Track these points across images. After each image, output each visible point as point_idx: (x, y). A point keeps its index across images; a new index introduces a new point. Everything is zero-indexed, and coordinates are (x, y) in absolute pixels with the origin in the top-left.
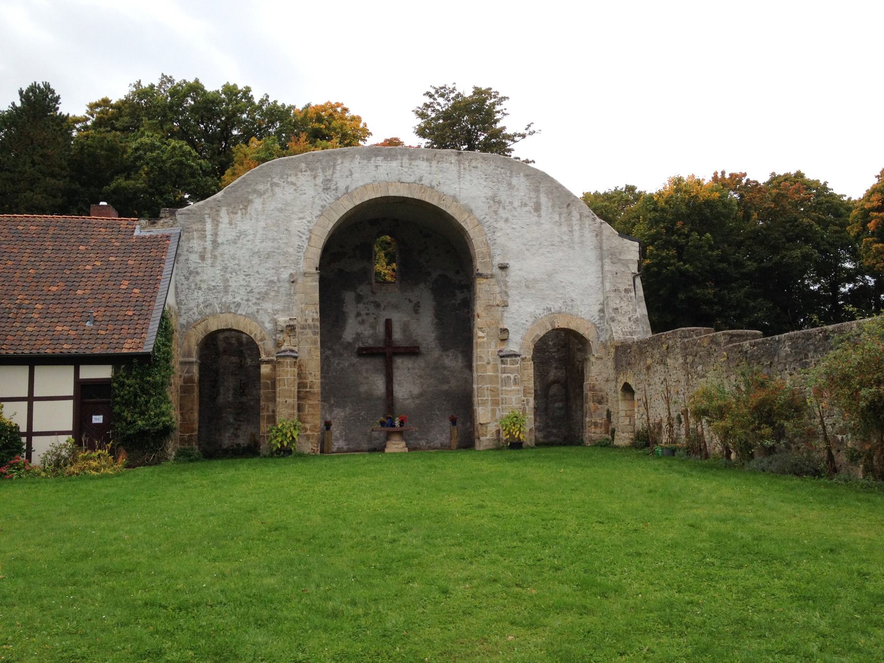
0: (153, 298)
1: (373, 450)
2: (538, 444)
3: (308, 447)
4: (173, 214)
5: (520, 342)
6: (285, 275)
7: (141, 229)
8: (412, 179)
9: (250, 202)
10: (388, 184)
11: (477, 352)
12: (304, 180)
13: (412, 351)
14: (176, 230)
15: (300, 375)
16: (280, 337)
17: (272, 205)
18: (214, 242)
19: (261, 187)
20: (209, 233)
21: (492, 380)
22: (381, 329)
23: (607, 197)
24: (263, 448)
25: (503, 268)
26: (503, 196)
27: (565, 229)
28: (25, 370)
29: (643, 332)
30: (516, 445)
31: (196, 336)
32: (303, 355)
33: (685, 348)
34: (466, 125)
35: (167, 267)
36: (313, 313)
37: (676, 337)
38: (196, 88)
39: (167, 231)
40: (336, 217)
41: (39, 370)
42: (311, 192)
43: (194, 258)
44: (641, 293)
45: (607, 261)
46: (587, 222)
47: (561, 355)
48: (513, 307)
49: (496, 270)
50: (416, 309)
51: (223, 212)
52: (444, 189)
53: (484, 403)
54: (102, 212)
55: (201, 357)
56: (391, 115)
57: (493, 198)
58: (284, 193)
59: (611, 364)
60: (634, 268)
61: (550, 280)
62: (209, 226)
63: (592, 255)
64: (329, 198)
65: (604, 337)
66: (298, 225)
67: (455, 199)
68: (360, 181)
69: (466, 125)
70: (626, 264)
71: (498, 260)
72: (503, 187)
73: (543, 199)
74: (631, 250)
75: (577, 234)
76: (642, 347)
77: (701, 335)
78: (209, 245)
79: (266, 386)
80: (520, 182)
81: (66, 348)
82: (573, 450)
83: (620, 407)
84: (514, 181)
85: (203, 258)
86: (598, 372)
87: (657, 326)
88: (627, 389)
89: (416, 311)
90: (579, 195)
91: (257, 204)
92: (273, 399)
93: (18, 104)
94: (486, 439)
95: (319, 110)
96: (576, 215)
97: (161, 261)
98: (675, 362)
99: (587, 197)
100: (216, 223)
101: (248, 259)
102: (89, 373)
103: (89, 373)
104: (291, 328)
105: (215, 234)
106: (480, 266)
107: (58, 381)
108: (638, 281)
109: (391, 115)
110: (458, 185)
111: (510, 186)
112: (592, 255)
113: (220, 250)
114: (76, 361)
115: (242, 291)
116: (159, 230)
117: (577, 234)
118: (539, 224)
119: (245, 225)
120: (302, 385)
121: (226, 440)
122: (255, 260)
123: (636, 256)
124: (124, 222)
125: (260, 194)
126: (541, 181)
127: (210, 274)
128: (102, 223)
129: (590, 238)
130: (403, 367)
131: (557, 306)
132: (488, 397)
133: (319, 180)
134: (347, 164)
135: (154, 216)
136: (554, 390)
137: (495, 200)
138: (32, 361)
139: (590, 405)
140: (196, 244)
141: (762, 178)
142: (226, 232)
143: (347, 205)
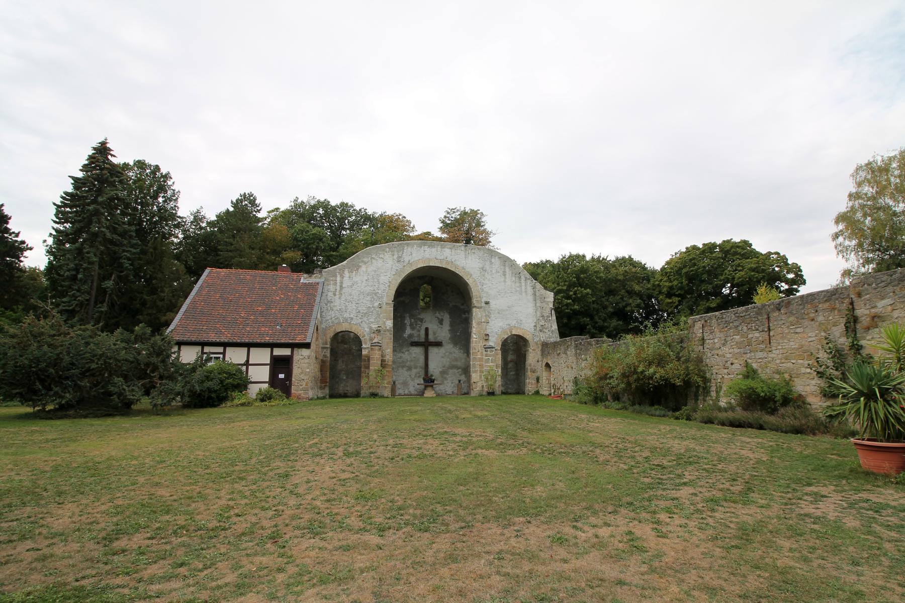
0: (311, 315)
1: (465, 394)
2: (503, 393)
3: (387, 392)
4: (321, 272)
5: (495, 341)
6: (376, 304)
7: (304, 279)
8: (442, 258)
9: (360, 267)
10: (430, 260)
11: (473, 345)
12: (387, 256)
13: (438, 344)
14: (323, 280)
15: (382, 356)
16: (373, 335)
17: (371, 269)
18: (341, 286)
19: (365, 260)
20: (338, 282)
21: (481, 360)
22: (423, 332)
23: (537, 266)
24: (362, 393)
25: (487, 303)
26: (487, 267)
27: (518, 284)
28: (246, 349)
29: (555, 337)
30: (491, 394)
31: (331, 334)
32: (384, 346)
33: (576, 346)
34: (465, 229)
35: (318, 299)
36: (390, 324)
37: (571, 340)
38: (325, 205)
39: (317, 280)
40: (403, 276)
41: (228, 349)
42: (391, 263)
43: (330, 294)
44: (554, 318)
45: (538, 301)
46: (529, 281)
47: (515, 348)
48: (491, 323)
49: (483, 305)
50: (441, 322)
51: (346, 272)
52: (458, 263)
53: (476, 372)
54: (284, 269)
55: (331, 345)
56: (426, 220)
57: (482, 268)
58: (377, 263)
59: (539, 353)
60: (551, 306)
61: (511, 310)
62: (338, 279)
63: (530, 298)
64: (400, 266)
65: (537, 339)
66: (384, 279)
67: (463, 268)
68: (419, 257)
69: (465, 229)
70: (547, 303)
71: (484, 300)
72: (488, 263)
73: (507, 269)
74: (550, 296)
75: (523, 287)
76: (555, 344)
77: (584, 339)
78: (338, 288)
79: (365, 360)
80: (496, 261)
81: (267, 339)
82: (520, 397)
83: (544, 375)
84: (493, 260)
85: (335, 295)
86: (533, 357)
87: (562, 335)
88: (548, 365)
89: (442, 324)
90: (521, 262)
91: (363, 268)
92: (368, 368)
93: (231, 209)
94: (476, 389)
95: (391, 218)
96: (523, 277)
97: (315, 296)
98: (571, 352)
99: (526, 266)
100: (342, 277)
101: (357, 297)
102: (278, 352)
103: (278, 352)
104: (379, 331)
105: (341, 283)
106: (474, 301)
107: (262, 356)
108: (553, 312)
109: (426, 220)
110: (461, 261)
111: (491, 263)
112: (531, 298)
113: (344, 290)
114: (272, 346)
115: (354, 312)
116: (313, 279)
117: (523, 287)
118: (505, 281)
119: (357, 278)
120: (383, 361)
121: (341, 389)
122: (361, 297)
123: (552, 300)
124: (295, 276)
125: (365, 263)
126: (505, 260)
127: (338, 303)
128: (284, 276)
129: (530, 291)
130: (433, 352)
131: (513, 323)
132: (478, 369)
133: (395, 257)
134: (409, 249)
135: (309, 272)
136: (510, 365)
137: (483, 269)
138: (249, 346)
139: (529, 373)
140: (332, 288)
141: (612, 258)
142: (347, 282)
143: (408, 270)
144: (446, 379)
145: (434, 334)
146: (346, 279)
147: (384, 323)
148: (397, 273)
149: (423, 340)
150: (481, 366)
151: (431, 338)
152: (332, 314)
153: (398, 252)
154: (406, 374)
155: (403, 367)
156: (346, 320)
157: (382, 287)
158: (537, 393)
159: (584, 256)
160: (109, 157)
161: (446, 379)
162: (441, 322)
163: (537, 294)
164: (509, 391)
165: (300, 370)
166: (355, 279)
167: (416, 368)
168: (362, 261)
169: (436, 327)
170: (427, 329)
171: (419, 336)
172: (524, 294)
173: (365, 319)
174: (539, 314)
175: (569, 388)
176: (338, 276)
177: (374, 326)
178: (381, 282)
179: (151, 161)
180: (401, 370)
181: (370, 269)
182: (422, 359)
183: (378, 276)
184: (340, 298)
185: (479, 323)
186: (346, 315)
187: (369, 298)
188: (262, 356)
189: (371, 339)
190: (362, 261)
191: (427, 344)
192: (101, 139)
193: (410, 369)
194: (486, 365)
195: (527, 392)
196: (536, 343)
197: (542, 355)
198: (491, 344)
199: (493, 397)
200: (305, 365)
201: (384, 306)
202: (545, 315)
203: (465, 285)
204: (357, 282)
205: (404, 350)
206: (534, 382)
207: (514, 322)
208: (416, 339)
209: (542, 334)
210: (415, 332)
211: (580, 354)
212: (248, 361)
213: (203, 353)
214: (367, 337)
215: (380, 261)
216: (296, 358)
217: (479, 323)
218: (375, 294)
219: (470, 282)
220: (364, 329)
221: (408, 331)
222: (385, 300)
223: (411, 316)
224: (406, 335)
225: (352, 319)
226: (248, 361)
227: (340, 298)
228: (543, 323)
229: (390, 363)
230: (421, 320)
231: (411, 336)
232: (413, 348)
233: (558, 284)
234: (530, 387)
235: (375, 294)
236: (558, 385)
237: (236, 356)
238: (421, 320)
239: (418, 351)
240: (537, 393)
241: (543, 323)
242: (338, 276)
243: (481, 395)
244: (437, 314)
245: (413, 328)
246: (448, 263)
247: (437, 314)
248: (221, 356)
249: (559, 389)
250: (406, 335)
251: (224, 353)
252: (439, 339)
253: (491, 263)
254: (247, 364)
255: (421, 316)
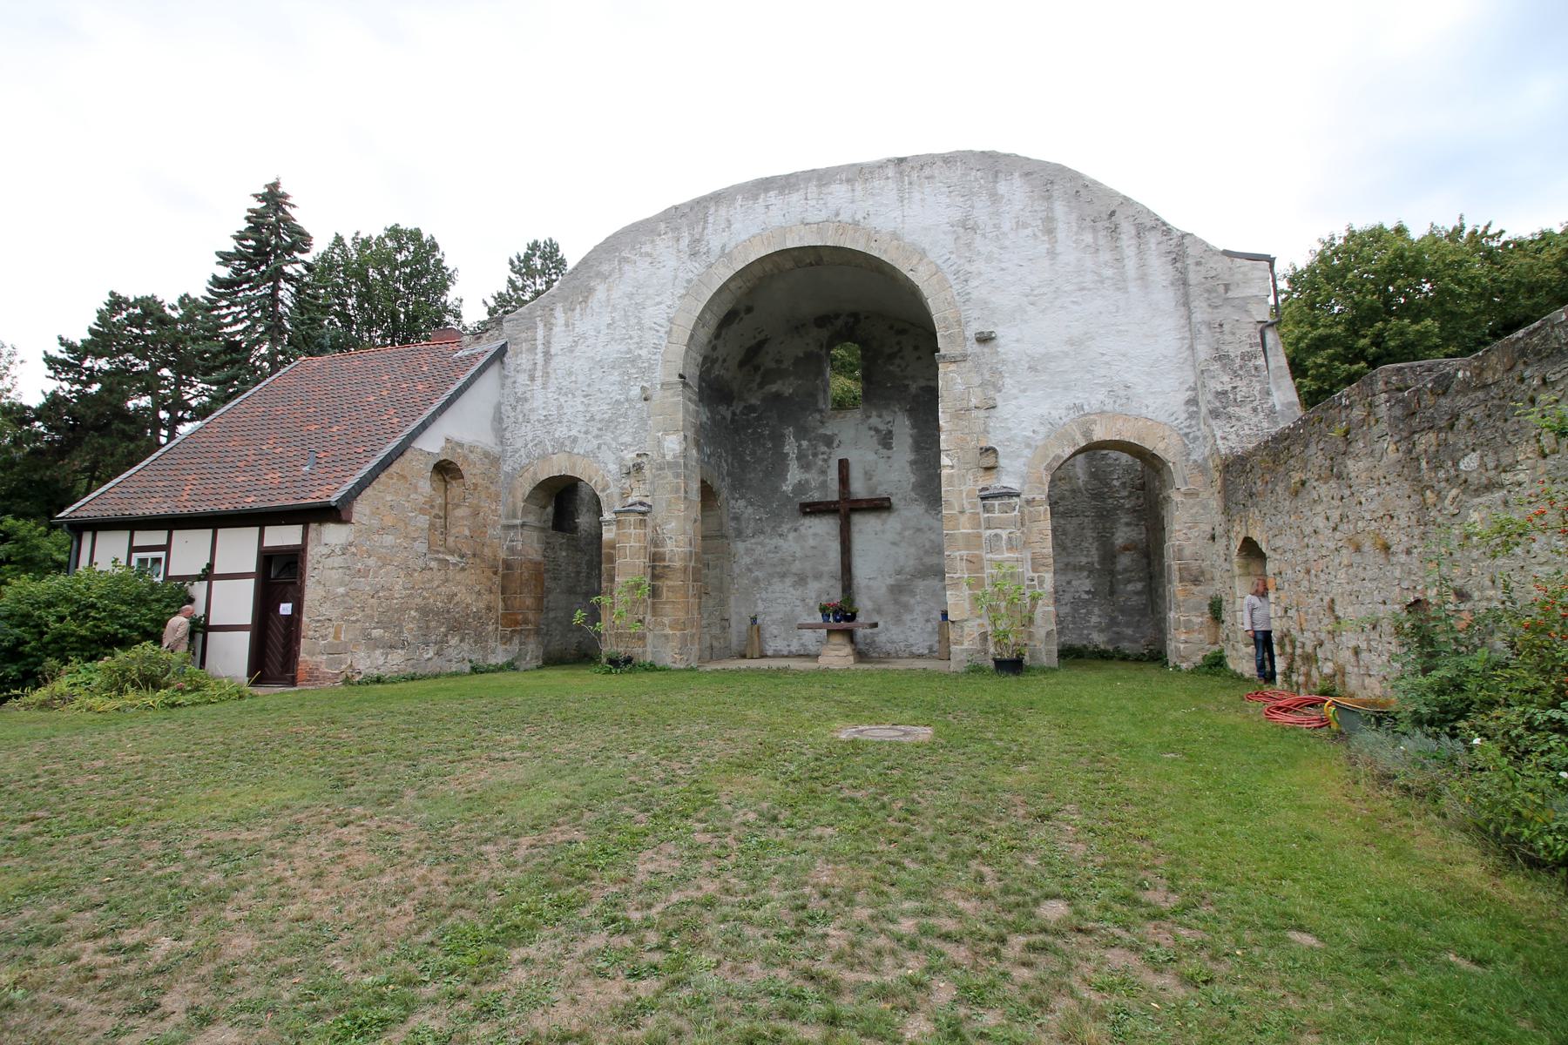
2: (1071, 655)
5: (1021, 472)
6: (635, 392)
8: (823, 216)
9: (591, 290)
10: (784, 231)
13: (880, 506)
16: (627, 483)
18: (547, 353)
20: (539, 342)
22: (834, 474)
25: (985, 339)
26: (981, 214)
27: (1105, 256)
30: (1012, 666)
31: (525, 486)
41: (176, 533)
43: (523, 378)
47: (1112, 499)
48: (1005, 409)
49: (973, 347)
50: (886, 440)
52: (876, 222)
59: (1215, 503)
62: (540, 333)
64: (697, 267)
66: (655, 314)
71: (971, 332)
73: (1060, 209)
75: (1131, 264)
78: (540, 358)
81: (251, 502)
84: (1002, 187)
85: (532, 379)
86: (1191, 524)
88: (1251, 549)
91: (600, 292)
92: (612, 579)
100: (549, 327)
104: (638, 468)
105: (547, 343)
107: (240, 550)
111: (995, 197)
112: (1165, 297)
113: (553, 364)
117: (1131, 264)
118: (1052, 254)
119: (584, 325)
120: (656, 558)
122: (597, 374)
125: (605, 278)
130: (866, 528)
131: (1095, 399)
136: (1124, 561)
137: (968, 225)
138: (214, 521)
143: (723, 274)
144: (907, 608)
145: (868, 476)
146: (558, 329)
147: (659, 442)
148: (691, 288)
149: (833, 495)
150: (974, 563)
151: (859, 489)
152: (527, 432)
153: (691, 226)
154: (794, 594)
155: (783, 576)
156: (560, 445)
157: (650, 338)
158: (1216, 663)
159: (1400, 230)
160: (287, 208)
161: (907, 608)
162: (886, 440)
163: (1193, 278)
164: (1126, 647)
165: (321, 592)
166: (581, 327)
167: (818, 576)
168: (598, 274)
169: (871, 456)
170: (844, 465)
171: (824, 485)
172: (1133, 288)
173: (608, 437)
174: (1204, 352)
175: (1377, 671)
176: (540, 325)
177: (630, 456)
178: (647, 323)
179: (407, 224)
180: (777, 586)
181: (615, 294)
182: (835, 547)
183: (640, 307)
184: (545, 386)
185: (959, 414)
186: (561, 432)
187: (615, 376)
188: (240, 550)
189: (624, 495)
190: (598, 274)
191: (846, 509)
192: (271, 181)
193: (801, 580)
194: (998, 561)
195: (1172, 659)
196: (1202, 468)
197: (1226, 510)
198: (1009, 481)
199: (1011, 680)
200: (336, 575)
201: (657, 395)
202: (1234, 351)
203: (910, 295)
204: (584, 337)
205: (785, 528)
206: (1200, 619)
207: (1101, 395)
208: (816, 496)
209: (1219, 428)
210: (813, 478)
211: (1445, 455)
212: (211, 566)
213: (133, 549)
214: (614, 490)
215: (644, 264)
216: (313, 552)
217: (961, 413)
218: (633, 361)
219: (920, 277)
220: (601, 469)
221: (794, 475)
222: (659, 375)
223: (802, 433)
224: (787, 488)
225: (575, 440)
226: (211, 566)
227: (545, 386)
228: (1223, 381)
229: (678, 564)
230: (829, 441)
231: (801, 487)
232: (807, 521)
233: (1313, 325)
234: (1186, 638)
235: (633, 361)
236: (1308, 639)
237: (188, 553)
238: (829, 441)
239: (823, 530)
240: (1216, 663)
241: (1223, 381)
242: (540, 325)
243: (976, 670)
244: (874, 421)
245: (806, 466)
246: (841, 227)
247: (874, 421)
248: (162, 554)
249: (1309, 659)
250: (787, 488)
251: (166, 548)
252: (881, 492)
253: (995, 197)
254: (208, 575)
255: (828, 431)
